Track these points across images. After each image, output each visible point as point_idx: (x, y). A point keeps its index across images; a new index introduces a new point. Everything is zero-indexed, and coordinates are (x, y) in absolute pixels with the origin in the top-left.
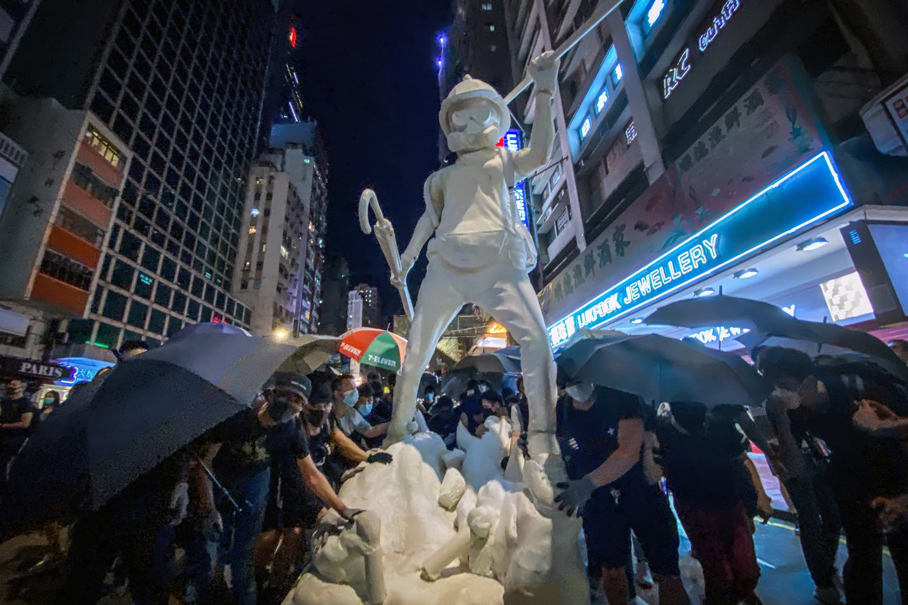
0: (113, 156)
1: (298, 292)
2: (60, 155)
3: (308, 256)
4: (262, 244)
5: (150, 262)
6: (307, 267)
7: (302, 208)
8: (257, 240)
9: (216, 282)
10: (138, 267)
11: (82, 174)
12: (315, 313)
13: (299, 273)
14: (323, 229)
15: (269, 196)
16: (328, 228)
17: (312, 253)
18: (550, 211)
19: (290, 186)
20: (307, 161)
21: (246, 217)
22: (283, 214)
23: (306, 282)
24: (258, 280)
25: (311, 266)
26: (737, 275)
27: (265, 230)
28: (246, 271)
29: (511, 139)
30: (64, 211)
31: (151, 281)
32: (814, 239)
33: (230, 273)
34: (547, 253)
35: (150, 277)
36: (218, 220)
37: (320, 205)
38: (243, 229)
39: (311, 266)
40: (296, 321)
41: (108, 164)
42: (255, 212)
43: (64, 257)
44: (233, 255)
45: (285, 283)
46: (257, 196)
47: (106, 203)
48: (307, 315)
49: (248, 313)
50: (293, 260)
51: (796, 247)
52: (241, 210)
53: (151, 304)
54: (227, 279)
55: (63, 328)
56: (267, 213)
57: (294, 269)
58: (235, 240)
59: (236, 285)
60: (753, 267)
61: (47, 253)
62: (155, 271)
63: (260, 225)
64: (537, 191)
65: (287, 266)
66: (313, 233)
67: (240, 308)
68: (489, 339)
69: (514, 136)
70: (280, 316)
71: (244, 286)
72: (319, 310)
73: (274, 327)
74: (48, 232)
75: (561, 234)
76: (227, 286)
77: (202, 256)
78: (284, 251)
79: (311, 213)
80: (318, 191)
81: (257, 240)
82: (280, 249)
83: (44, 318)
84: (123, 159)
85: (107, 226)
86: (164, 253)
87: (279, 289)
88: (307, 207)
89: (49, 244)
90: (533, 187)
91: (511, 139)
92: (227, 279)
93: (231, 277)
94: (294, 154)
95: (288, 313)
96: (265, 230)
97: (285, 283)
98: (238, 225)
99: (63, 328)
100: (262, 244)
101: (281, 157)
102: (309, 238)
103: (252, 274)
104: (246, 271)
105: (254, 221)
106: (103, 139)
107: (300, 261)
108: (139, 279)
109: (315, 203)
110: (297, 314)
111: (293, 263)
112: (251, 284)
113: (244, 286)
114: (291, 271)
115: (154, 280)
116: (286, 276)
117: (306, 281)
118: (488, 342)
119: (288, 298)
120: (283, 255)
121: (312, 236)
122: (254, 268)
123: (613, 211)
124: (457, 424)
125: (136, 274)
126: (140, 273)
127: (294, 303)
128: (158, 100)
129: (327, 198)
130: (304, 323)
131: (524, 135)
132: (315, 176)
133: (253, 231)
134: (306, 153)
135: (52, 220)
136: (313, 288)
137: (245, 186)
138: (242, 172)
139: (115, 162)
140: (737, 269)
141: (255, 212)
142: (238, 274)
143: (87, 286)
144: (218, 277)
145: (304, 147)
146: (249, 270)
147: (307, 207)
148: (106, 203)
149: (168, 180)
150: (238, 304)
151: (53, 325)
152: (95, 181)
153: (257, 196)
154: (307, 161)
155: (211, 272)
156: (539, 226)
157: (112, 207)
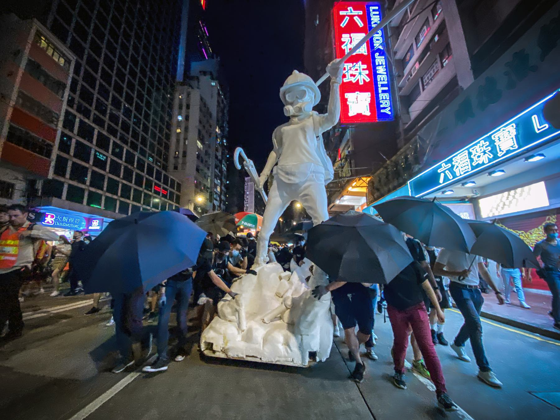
0: (60, 58)
1: (212, 173)
2: (18, 53)
3: (217, 150)
4: (185, 139)
5: (103, 143)
6: (216, 157)
7: (211, 115)
8: (182, 137)
9: (156, 164)
10: (94, 147)
11: (34, 68)
12: (223, 188)
13: (212, 162)
14: (226, 133)
15: (188, 107)
16: (229, 132)
17: (220, 149)
18: (417, 66)
19: (202, 99)
20: (213, 84)
21: (174, 122)
22: (197, 118)
23: (216, 167)
24: (184, 163)
25: (220, 157)
26: (443, 192)
27: (186, 129)
28: (176, 158)
29: (374, 10)
30: (21, 95)
31: (105, 158)
32: (535, 155)
33: (166, 159)
34: (408, 113)
35: (104, 155)
36: (154, 122)
37: (223, 114)
38: (173, 129)
39: (220, 157)
40: (211, 193)
41: (57, 64)
42: (180, 118)
43: (41, 139)
44: (167, 147)
45: (202, 166)
46: (180, 107)
47: (57, 93)
48: (219, 189)
49: (179, 185)
50: (206, 151)
51: (487, 174)
52: (170, 116)
53: (107, 174)
54: (165, 163)
55: (39, 185)
56: (187, 118)
57: (207, 157)
58: (168, 137)
59: (171, 167)
60: (472, 180)
61: (11, 128)
62: (107, 151)
63: (183, 126)
64: (399, 56)
65: (203, 155)
66: (219, 134)
67: (173, 181)
68: (346, 197)
69: (377, 8)
70: (199, 188)
71: (176, 168)
72: (227, 187)
73: (195, 194)
74: (10, 111)
75: (427, 88)
76: (165, 168)
77: (146, 146)
78: (199, 144)
79: (218, 121)
80: (222, 105)
81: (182, 137)
82: (196, 143)
83: (24, 178)
84: (68, 61)
85: (60, 111)
86: (137, 155)
87: (198, 170)
88: (214, 114)
89: (12, 120)
90: (395, 53)
91: (374, 10)
92: (165, 163)
93: (167, 162)
94: (205, 79)
95: (205, 186)
96: (186, 129)
97: (202, 166)
98: (169, 126)
99: (39, 185)
100: (185, 139)
101: (196, 82)
102: (217, 137)
103: (180, 161)
104: (176, 158)
105: (179, 124)
106: (49, 43)
107: (212, 152)
108: (95, 155)
109: (220, 115)
110: (211, 188)
111: (207, 153)
112: (180, 167)
113: (176, 168)
114: (205, 158)
115: (107, 157)
116: (202, 161)
117: (216, 167)
118: (344, 201)
119: (205, 177)
120: (199, 147)
121: (219, 136)
122: (181, 156)
123: (431, 113)
124: (363, 286)
125: (93, 152)
126: (96, 151)
127: (209, 180)
128: (90, 12)
129: (228, 111)
130: (216, 193)
131: (386, 6)
132: (219, 94)
133: (179, 131)
134: (213, 79)
135: (12, 103)
136: (221, 171)
137: (172, 99)
138: (169, 90)
139: (62, 61)
140: (443, 190)
141: (180, 118)
142: (171, 160)
143: (49, 155)
144: (157, 161)
145: (211, 74)
146: (178, 157)
147: (214, 114)
148: (57, 93)
149: (145, 118)
150: (171, 179)
151: (31, 184)
152: (47, 76)
153: (180, 107)
154: (213, 84)
155: (152, 157)
156: (400, 89)
157: (62, 97)
